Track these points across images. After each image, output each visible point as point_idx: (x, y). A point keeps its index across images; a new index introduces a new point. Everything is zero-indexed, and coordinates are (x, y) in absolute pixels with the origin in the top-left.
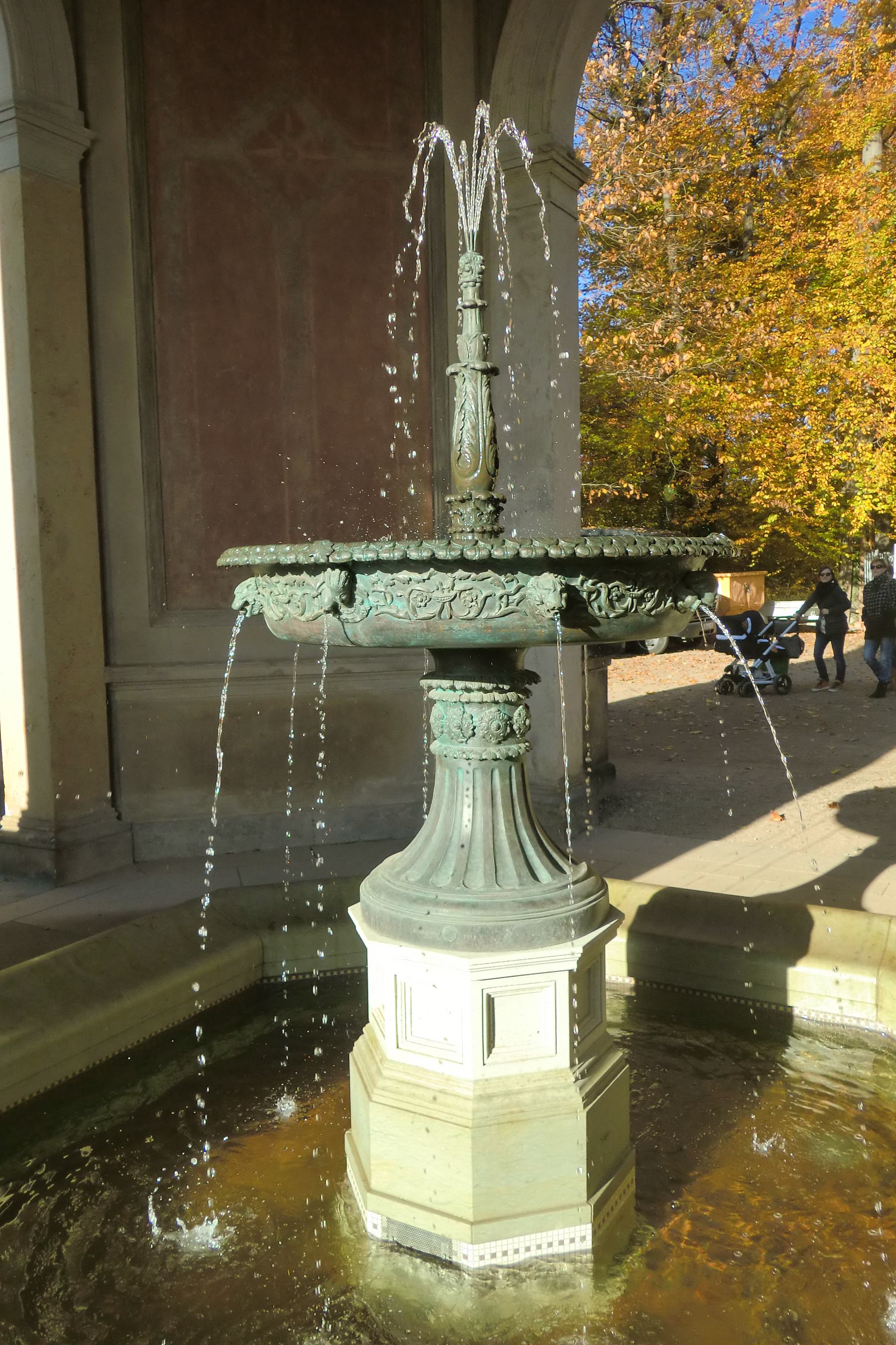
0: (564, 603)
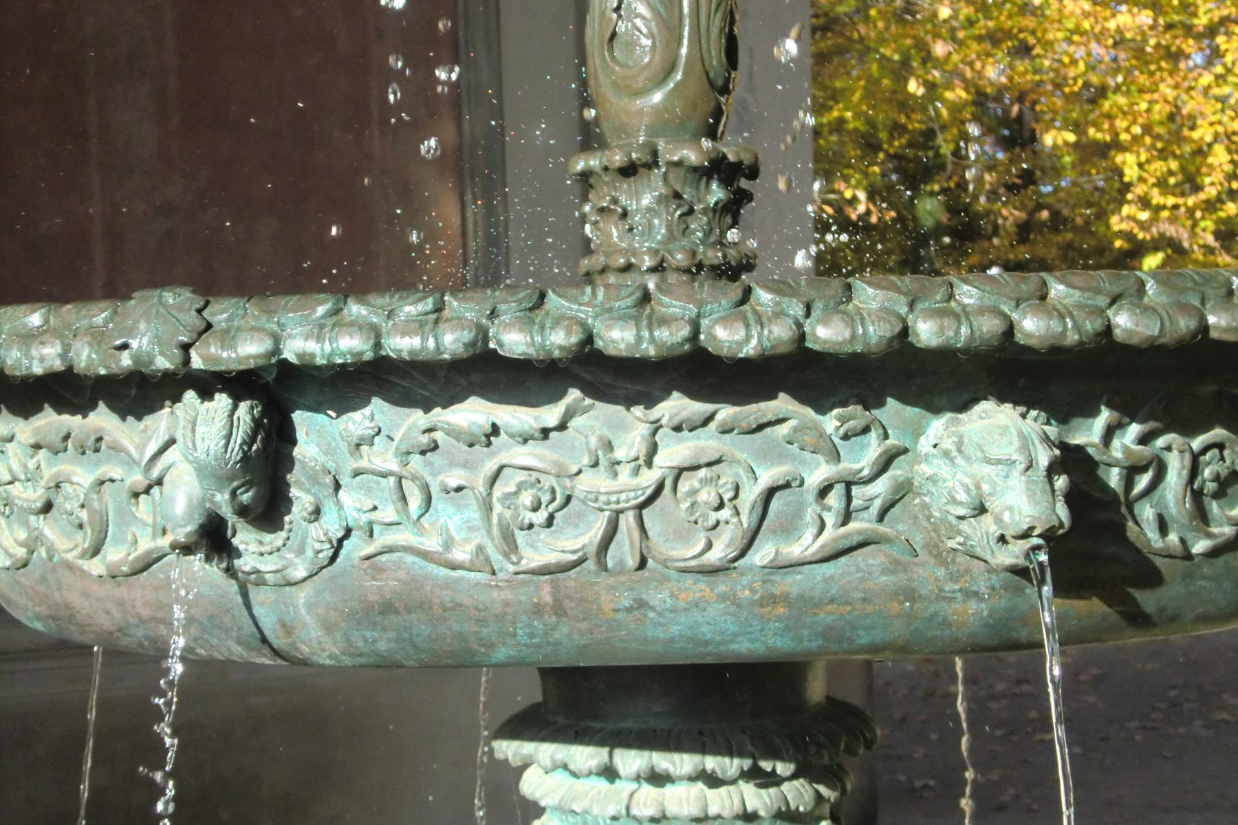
0: (1062, 512)
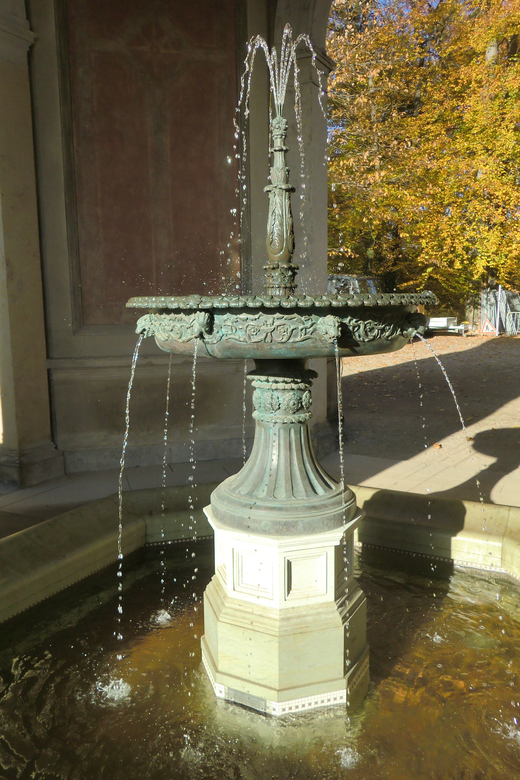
0: (340, 333)
